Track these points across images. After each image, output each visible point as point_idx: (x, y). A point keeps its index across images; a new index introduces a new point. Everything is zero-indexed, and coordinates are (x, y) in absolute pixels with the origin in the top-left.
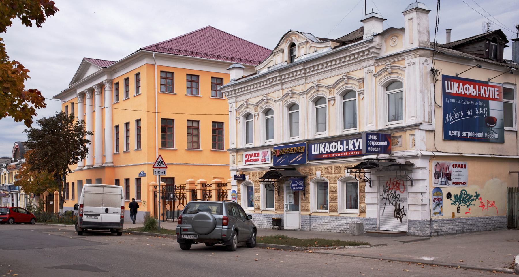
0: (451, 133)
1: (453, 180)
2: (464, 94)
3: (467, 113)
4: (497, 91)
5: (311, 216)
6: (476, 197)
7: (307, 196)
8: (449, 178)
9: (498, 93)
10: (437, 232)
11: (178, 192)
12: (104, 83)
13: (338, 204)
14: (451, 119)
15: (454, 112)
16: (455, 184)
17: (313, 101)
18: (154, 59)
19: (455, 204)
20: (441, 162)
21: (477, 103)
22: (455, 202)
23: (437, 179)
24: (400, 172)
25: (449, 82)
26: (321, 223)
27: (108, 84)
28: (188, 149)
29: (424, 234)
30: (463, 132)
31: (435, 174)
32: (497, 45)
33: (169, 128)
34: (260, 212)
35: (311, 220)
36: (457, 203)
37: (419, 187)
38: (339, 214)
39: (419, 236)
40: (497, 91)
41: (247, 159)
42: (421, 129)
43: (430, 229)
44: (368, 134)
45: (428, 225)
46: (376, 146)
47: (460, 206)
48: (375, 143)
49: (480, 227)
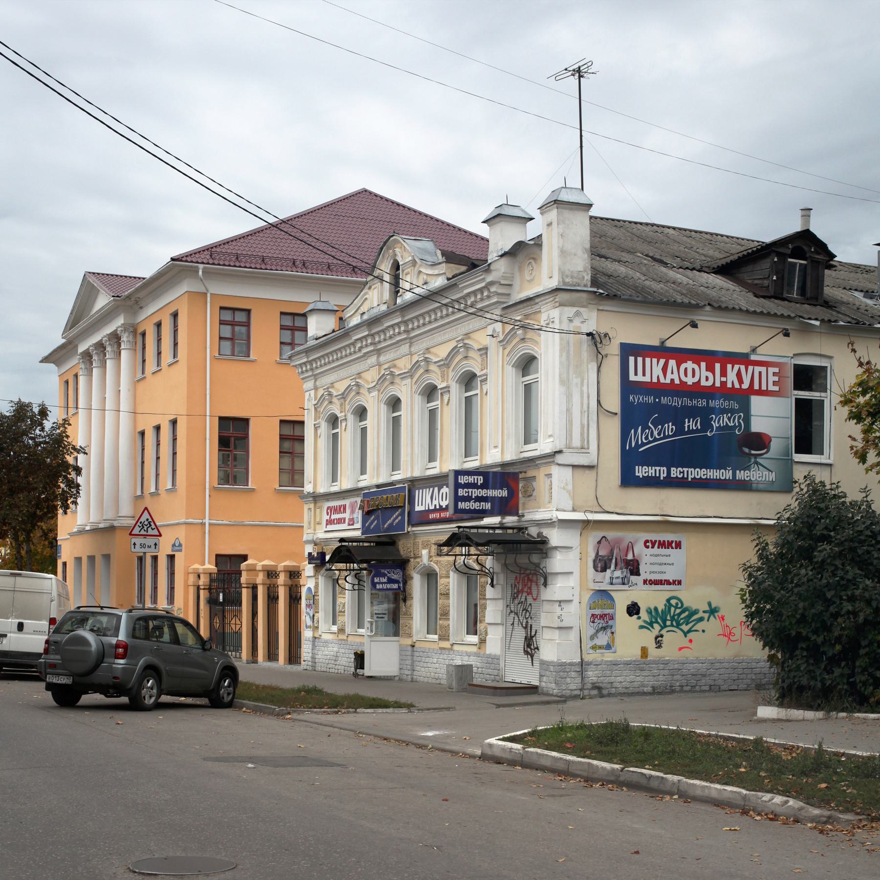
0: (641, 472)
1: (644, 576)
2: (679, 383)
3: (686, 425)
4: (774, 374)
5: (415, 649)
6: (708, 614)
7: (408, 603)
8: (633, 569)
9: (776, 379)
10: (599, 689)
12: (118, 332)
13: (451, 622)
14: (642, 439)
15: (650, 425)
16: (651, 584)
17: (422, 393)
18: (202, 280)
19: (651, 628)
20: (612, 535)
21: (715, 404)
22: (651, 624)
23: (602, 571)
24: (515, 555)
25: (640, 359)
26: (429, 665)
27: (126, 334)
28: (281, 488)
29: (564, 691)
30: (675, 469)
31: (594, 561)
32: (806, 265)
33: (237, 439)
34: (346, 638)
35: (415, 658)
36: (655, 625)
37: (558, 589)
38: (452, 645)
39: (552, 695)
40: (774, 374)
41: (328, 517)
42: (560, 462)
43: (580, 681)
44: (458, 473)
45: (573, 673)
46: (479, 499)
47: (664, 632)
48: (476, 493)
49: (720, 682)
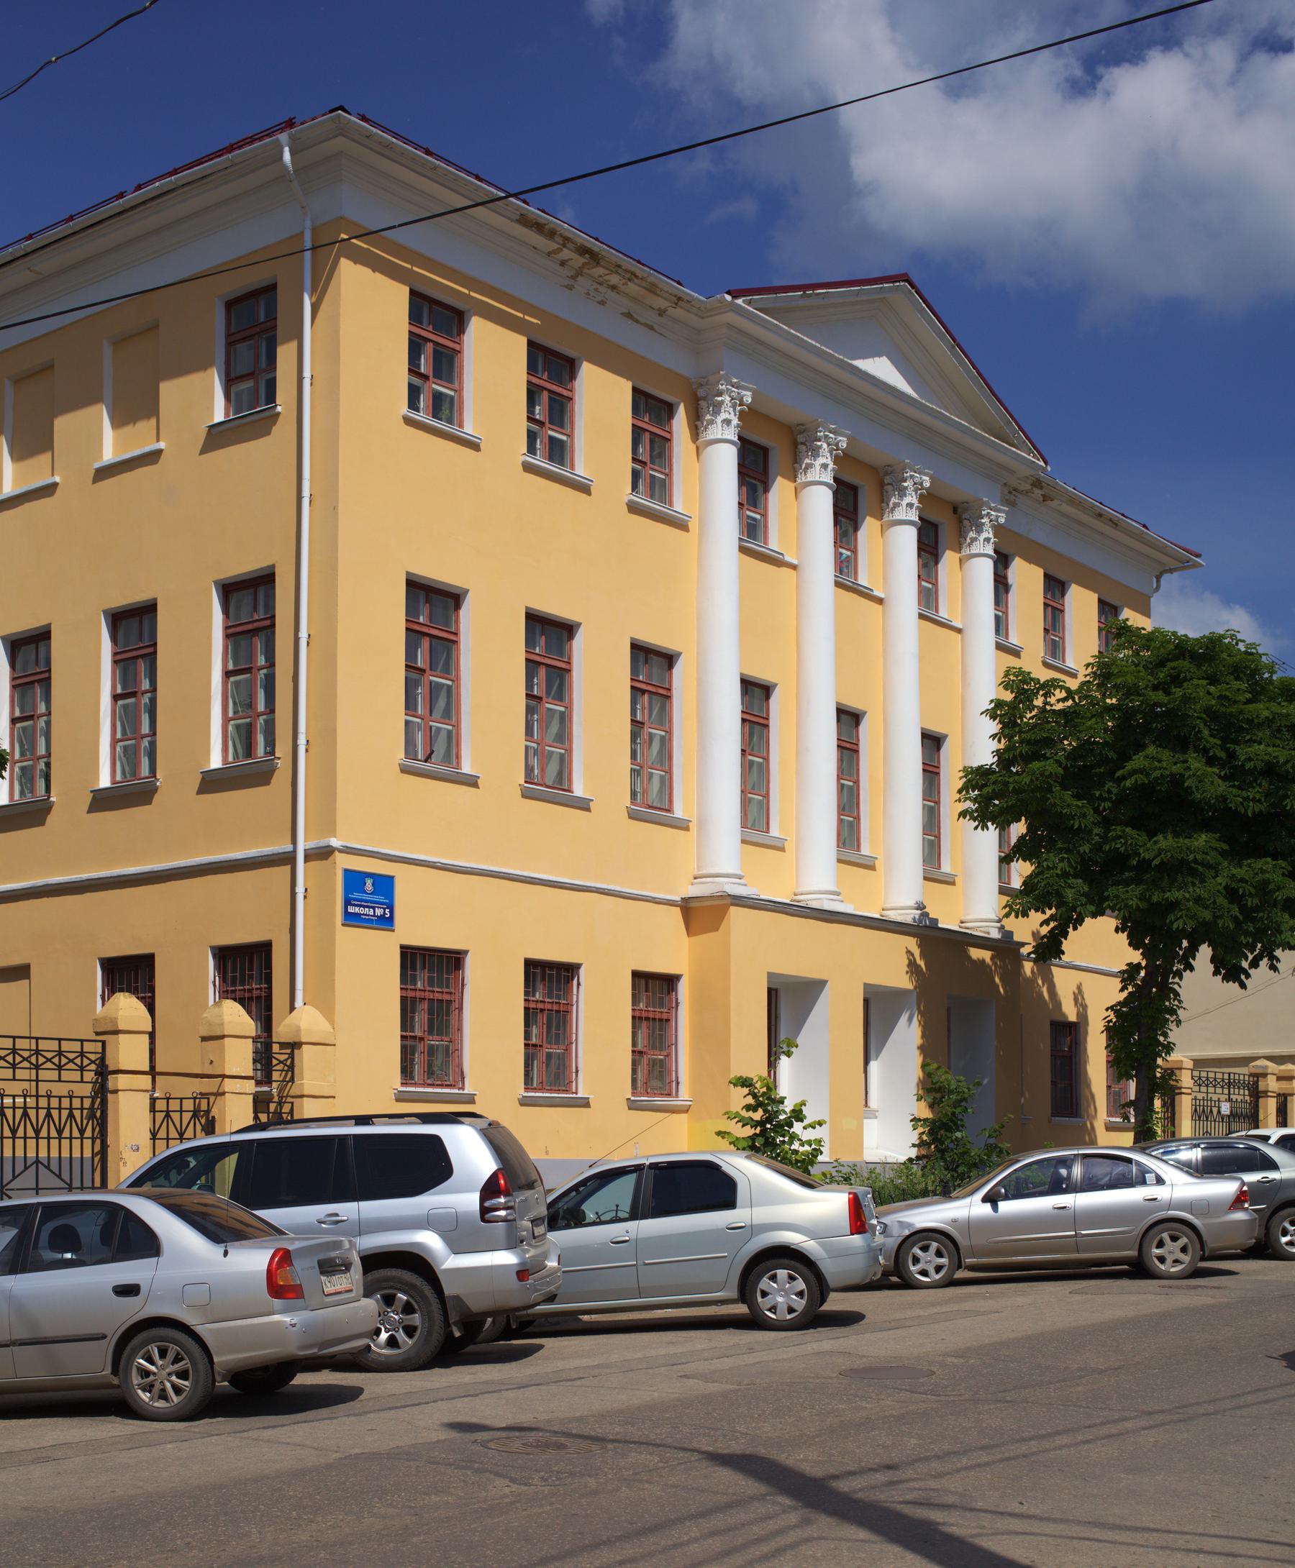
11: (1240, 1098)
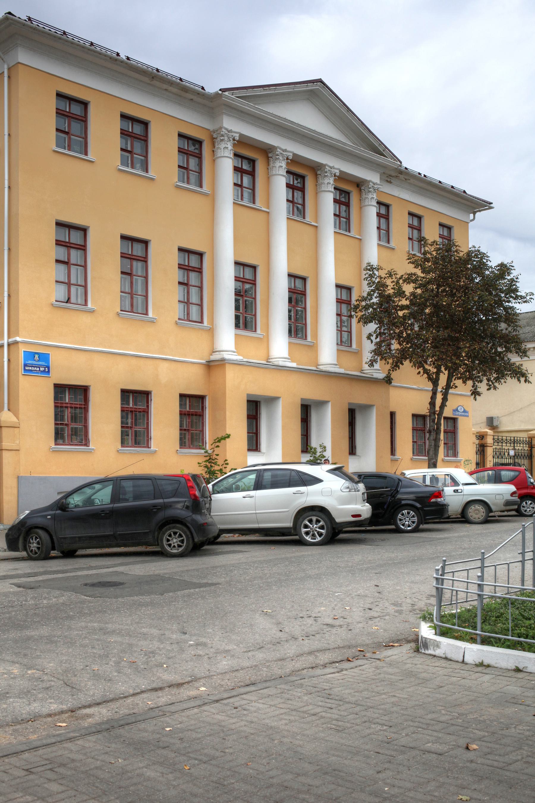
11: (520, 448)
